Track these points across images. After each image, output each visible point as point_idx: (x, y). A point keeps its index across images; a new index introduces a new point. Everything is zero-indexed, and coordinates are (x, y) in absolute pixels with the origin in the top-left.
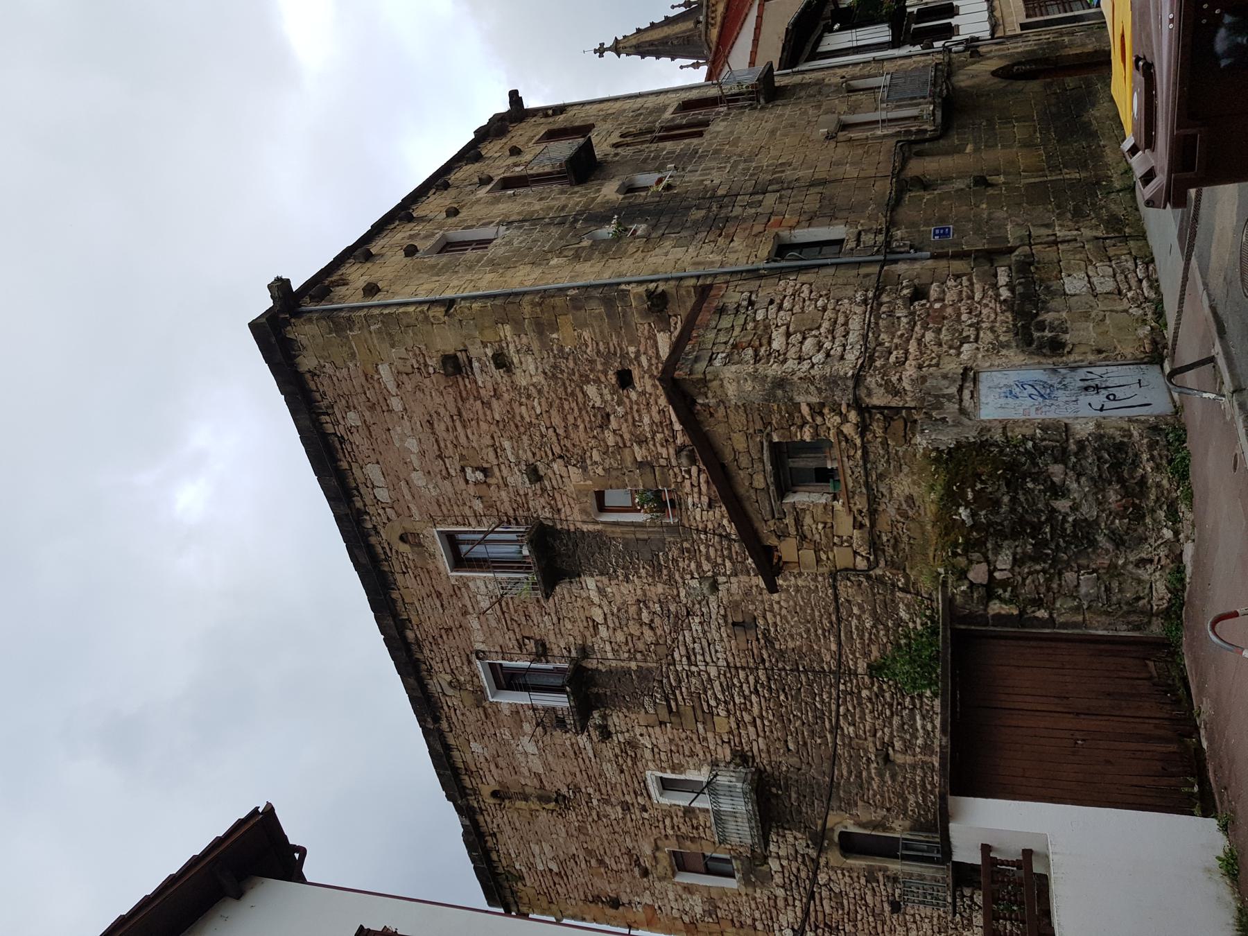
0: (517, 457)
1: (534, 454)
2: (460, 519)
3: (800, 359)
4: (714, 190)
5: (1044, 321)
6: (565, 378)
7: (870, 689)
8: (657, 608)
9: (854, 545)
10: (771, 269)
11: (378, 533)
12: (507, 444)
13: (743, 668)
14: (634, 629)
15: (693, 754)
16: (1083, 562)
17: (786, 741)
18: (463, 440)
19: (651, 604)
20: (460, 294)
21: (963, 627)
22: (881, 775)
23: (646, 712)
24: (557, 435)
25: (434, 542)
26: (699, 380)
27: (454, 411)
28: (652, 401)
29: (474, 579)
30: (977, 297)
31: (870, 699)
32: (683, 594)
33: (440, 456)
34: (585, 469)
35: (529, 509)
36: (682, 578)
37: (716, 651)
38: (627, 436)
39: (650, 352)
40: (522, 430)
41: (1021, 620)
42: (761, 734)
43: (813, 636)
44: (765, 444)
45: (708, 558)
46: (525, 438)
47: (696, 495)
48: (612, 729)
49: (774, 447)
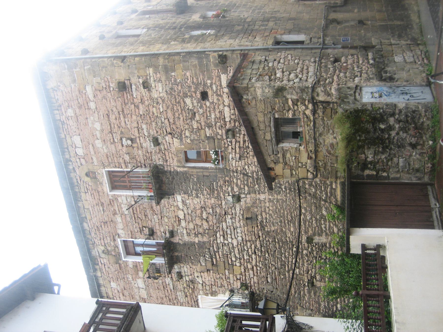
0: (149, 133)
1: (157, 132)
2: (117, 164)
3: (289, 81)
4: (245, 19)
5: (387, 71)
6: (176, 96)
7: (307, 250)
8: (211, 210)
9: (308, 167)
10: (274, 48)
11: (75, 171)
12: (144, 126)
13: (250, 241)
14: (198, 222)
15: (222, 286)
16: (401, 154)
17: (267, 278)
18: (123, 124)
19: (208, 209)
20: (129, 54)
21: (355, 181)
22: (309, 293)
23: (201, 265)
24: (169, 122)
25: (103, 176)
26: (245, 87)
27: (120, 109)
28: (216, 107)
29: (121, 196)
30: (360, 62)
31: (307, 255)
32: (224, 203)
33: (111, 132)
34: (181, 140)
35: (152, 160)
36: (224, 195)
37: (237, 233)
38: (203, 124)
39: (217, 83)
40: (153, 119)
41: (377, 177)
42: (256, 274)
43: (283, 224)
44: (272, 118)
45: (237, 185)
46: (154, 124)
47: (234, 154)
48: (183, 274)
49: (276, 120)
